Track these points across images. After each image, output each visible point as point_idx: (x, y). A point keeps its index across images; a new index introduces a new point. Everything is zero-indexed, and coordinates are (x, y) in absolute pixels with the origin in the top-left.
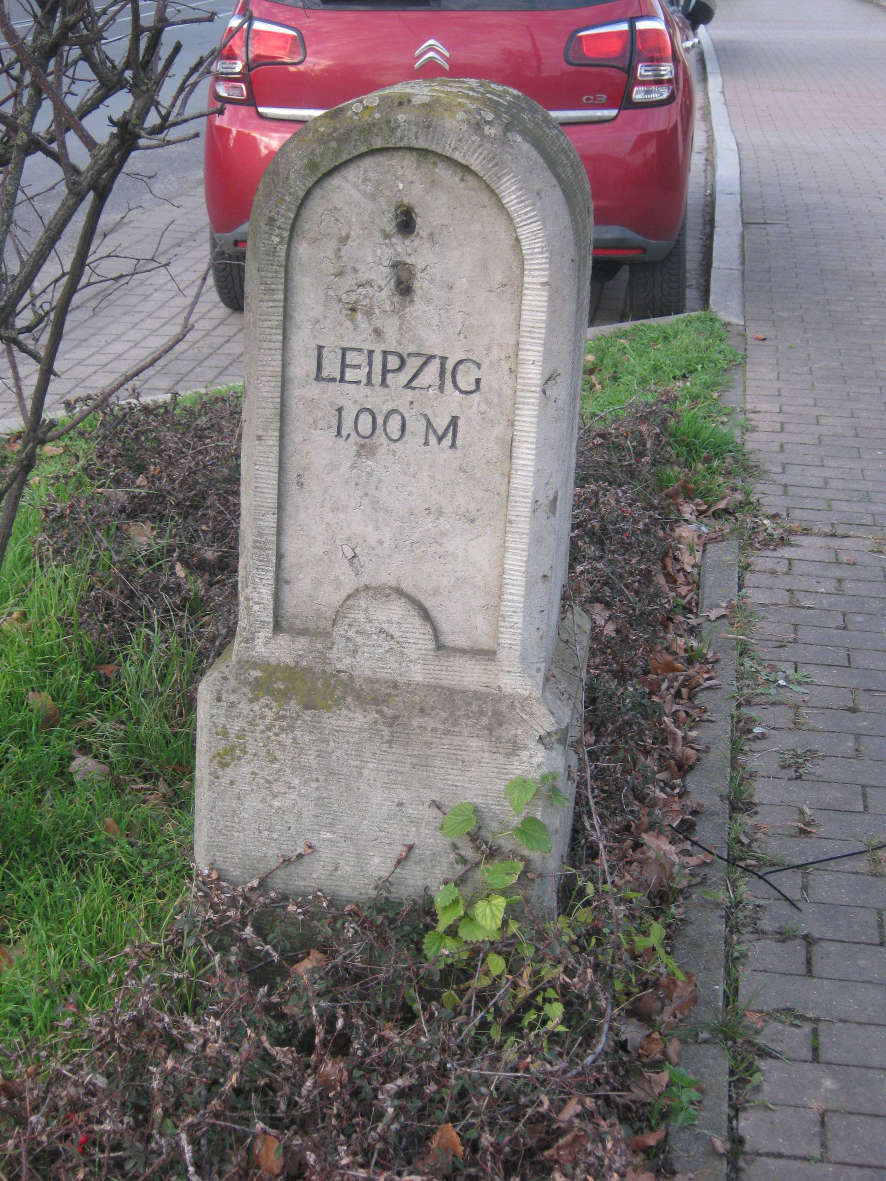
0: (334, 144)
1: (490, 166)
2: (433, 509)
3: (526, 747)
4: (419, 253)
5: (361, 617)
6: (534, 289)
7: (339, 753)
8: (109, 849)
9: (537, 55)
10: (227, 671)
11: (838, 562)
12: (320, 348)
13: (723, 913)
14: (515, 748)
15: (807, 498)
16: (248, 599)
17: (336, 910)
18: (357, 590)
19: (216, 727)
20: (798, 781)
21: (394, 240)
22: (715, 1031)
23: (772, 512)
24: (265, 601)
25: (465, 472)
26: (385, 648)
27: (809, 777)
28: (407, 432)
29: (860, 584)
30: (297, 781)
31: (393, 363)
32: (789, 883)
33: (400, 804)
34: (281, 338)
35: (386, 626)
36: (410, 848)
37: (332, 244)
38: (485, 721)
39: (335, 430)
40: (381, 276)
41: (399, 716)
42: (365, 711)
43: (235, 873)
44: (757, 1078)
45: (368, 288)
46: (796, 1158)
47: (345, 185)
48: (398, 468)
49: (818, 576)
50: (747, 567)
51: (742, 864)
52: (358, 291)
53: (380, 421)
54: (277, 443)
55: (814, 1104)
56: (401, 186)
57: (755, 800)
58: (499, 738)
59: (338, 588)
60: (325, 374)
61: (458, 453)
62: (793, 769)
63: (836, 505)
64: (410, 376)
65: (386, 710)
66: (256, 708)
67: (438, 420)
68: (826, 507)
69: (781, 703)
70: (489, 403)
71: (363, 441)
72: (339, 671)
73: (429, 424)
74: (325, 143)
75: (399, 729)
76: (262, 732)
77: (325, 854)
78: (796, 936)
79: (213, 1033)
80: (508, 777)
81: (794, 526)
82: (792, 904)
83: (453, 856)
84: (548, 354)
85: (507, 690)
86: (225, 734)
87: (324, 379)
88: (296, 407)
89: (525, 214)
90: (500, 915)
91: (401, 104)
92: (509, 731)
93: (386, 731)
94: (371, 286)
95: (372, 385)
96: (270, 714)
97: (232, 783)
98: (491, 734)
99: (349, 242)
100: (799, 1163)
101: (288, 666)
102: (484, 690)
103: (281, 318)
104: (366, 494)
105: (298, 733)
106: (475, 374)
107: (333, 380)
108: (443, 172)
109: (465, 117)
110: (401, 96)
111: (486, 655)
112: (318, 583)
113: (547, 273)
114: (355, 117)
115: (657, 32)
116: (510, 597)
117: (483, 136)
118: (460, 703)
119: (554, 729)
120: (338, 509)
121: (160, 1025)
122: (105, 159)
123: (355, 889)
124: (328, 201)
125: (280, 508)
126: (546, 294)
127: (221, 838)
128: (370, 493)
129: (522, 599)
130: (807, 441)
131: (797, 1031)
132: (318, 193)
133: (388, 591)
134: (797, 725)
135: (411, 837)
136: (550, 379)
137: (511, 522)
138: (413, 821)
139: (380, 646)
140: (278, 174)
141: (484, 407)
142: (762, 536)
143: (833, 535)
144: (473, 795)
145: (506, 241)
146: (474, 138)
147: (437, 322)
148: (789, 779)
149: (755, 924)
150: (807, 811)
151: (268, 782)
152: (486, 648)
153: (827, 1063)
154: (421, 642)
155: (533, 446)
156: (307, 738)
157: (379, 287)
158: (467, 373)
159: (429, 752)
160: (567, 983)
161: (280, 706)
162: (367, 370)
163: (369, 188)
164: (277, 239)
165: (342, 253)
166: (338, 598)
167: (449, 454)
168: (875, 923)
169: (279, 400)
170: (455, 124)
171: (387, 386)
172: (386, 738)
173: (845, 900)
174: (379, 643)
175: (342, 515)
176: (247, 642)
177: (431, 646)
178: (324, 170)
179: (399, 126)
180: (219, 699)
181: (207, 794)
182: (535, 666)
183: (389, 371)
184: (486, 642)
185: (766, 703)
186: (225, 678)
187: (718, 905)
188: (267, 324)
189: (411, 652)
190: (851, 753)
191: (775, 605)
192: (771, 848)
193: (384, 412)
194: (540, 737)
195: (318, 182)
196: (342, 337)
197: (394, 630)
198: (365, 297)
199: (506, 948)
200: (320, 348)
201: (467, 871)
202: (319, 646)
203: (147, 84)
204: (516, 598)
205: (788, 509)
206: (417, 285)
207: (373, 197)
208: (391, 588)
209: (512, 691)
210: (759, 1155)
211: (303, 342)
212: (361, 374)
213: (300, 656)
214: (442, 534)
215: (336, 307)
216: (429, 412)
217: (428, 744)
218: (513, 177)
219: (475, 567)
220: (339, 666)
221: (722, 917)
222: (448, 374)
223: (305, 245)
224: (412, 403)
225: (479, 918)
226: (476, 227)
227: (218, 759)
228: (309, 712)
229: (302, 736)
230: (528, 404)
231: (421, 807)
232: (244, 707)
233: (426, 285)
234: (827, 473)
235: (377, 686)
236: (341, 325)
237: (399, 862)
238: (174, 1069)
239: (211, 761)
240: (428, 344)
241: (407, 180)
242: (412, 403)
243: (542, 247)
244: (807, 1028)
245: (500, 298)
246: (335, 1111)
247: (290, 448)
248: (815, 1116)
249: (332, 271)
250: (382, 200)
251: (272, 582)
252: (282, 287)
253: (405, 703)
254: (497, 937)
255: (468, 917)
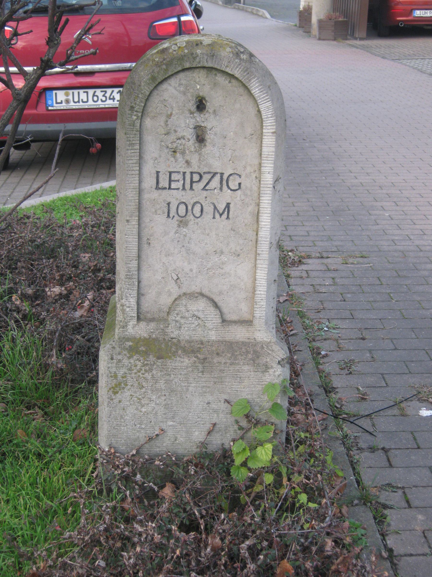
0: (164, 67)
1: (245, 74)
2: (218, 251)
3: (272, 367)
4: (208, 120)
5: (183, 309)
6: (268, 136)
7: (176, 380)
8: (25, 446)
9: (128, 35)
10: (114, 344)
11: (329, 270)
12: (158, 172)
13: (341, 442)
14: (267, 368)
15: (302, 241)
16: (122, 305)
17: (178, 461)
18: (180, 296)
19: (111, 373)
20: (351, 375)
21: (195, 115)
22: (360, 499)
23: (289, 249)
24: (133, 306)
25: (234, 231)
26: (196, 324)
27: (355, 373)
28: (204, 213)
29: (344, 279)
30: (154, 397)
31: (196, 177)
32: (365, 423)
33: (209, 403)
34: (138, 168)
35: (196, 313)
36: (214, 425)
37: (163, 119)
38: (250, 356)
39: (166, 214)
40: (190, 134)
41: (206, 358)
42: (189, 357)
43: (123, 448)
44: (388, 519)
45: (182, 140)
46: (419, 555)
47: (169, 88)
48: (199, 231)
49: (322, 277)
50: (288, 276)
51: (340, 417)
52: (177, 142)
53: (190, 208)
54: (137, 223)
55: (418, 528)
56: (198, 87)
57: (334, 386)
58: (259, 364)
59: (170, 295)
60: (160, 186)
61: (230, 221)
62: (346, 370)
63: (317, 243)
64: (205, 184)
65: (199, 355)
66: (132, 361)
67: (220, 205)
68: (313, 245)
69: (328, 339)
70: (246, 195)
71: (181, 219)
72: (172, 338)
73: (215, 208)
74: (159, 67)
75: (207, 364)
76: (136, 373)
77: (170, 433)
78: (378, 449)
79: (151, 531)
80: (263, 383)
81: (303, 254)
82: (371, 433)
83: (236, 427)
84: (276, 168)
85: (259, 339)
86: (115, 376)
87: (160, 189)
88: (146, 204)
89: (263, 98)
90: (270, 453)
91: (197, 45)
92: (263, 360)
93: (200, 367)
94: (184, 139)
95: (186, 190)
96: (139, 364)
97: (120, 402)
98: (254, 362)
99: (172, 117)
100: (422, 557)
101: (145, 338)
102: (247, 340)
103: (138, 158)
104: (183, 246)
105: (154, 372)
106: (238, 180)
107: (165, 188)
108: (221, 79)
109: (231, 50)
110: (197, 41)
111: (248, 323)
112: (159, 294)
113: (274, 127)
114: (174, 53)
115: (190, 22)
116: (259, 292)
117: (240, 59)
118: (236, 348)
119: (285, 356)
120: (169, 255)
121: (118, 530)
122: (34, 81)
123: (186, 449)
124: (160, 96)
125: (139, 257)
126: (274, 137)
127: (115, 431)
128: (185, 245)
129: (265, 293)
130: (292, 214)
131: (396, 494)
132: (155, 93)
133: (196, 295)
134: (340, 349)
135: (214, 420)
136: (277, 180)
137: (259, 255)
138: (216, 411)
139: (193, 323)
140: (134, 84)
141: (243, 197)
142: (290, 261)
143: (322, 257)
144: (245, 394)
145: (253, 111)
146: (236, 60)
147: (218, 155)
148: (346, 374)
149: (357, 445)
150: (361, 388)
151: (139, 399)
152: (247, 319)
153: (417, 508)
154: (215, 319)
155: (269, 215)
156: (159, 374)
157: (188, 139)
158: (234, 180)
159: (223, 375)
160: (307, 483)
161: (144, 359)
162: (182, 182)
163: (182, 89)
164: (135, 117)
165: (169, 123)
166: (170, 300)
167: (226, 222)
168: (412, 439)
169: (138, 201)
170: (226, 54)
171: (193, 190)
172: (201, 370)
173: (394, 429)
174: (193, 322)
175: (171, 258)
176: (123, 328)
177: (220, 321)
178: (159, 80)
179: (198, 56)
180: (112, 359)
181: (106, 409)
182: (271, 326)
183: (194, 182)
184: (246, 316)
185: (322, 340)
186: (114, 348)
187: (337, 438)
188: (131, 162)
189: (209, 325)
190: (370, 359)
191: (308, 292)
192: (350, 408)
193: (192, 203)
194: (279, 362)
195: (156, 87)
196: (169, 166)
197: (200, 315)
198: (181, 145)
199: (274, 469)
200: (158, 172)
201: (244, 433)
202: (162, 326)
203: (57, 40)
204: (262, 293)
205: (296, 247)
206: (207, 137)
207: (184, 93)
208: (197, 293)
209: (261, 340)
210: (401, 556)
211: (149, 169)
212: (180, 185)
213: (152, 332)
214: (223, 264)
215: (166, 151)
216: (215, 202)
217: (222, 371)
218: (257, 79)
219: (240, 278)
220: (172, 336)
221: (341, 444)
222: (224, 181)
223: (149, 120)
224: (206, 197)
225: (259, 456)
226: (238, 106)
227: (112, 390)
228: (160, 361)
229: (157, 373)
230: (267, 194)
231: (219, 404)
232: (126, 361)
233: (212, 136)
234: (307, 229)
235: (192, 344)
236: (169, 160)
237: (209, 433)
238: (141, 551)
239: (108, 391)
240: (214, 167)
241: (201, 83)
242: (206, 197)
243: (272, 114)
244: (400, 492)
245: (250, 141)
246: (224, 562)
247: (143, 225)
248: (420, 533)
249: (164, 133)
250: (189, 95)
251: (136, 295)
252: (138, 142)
253: (208, 351)
254: (269, 465)
255: (254, 457)
